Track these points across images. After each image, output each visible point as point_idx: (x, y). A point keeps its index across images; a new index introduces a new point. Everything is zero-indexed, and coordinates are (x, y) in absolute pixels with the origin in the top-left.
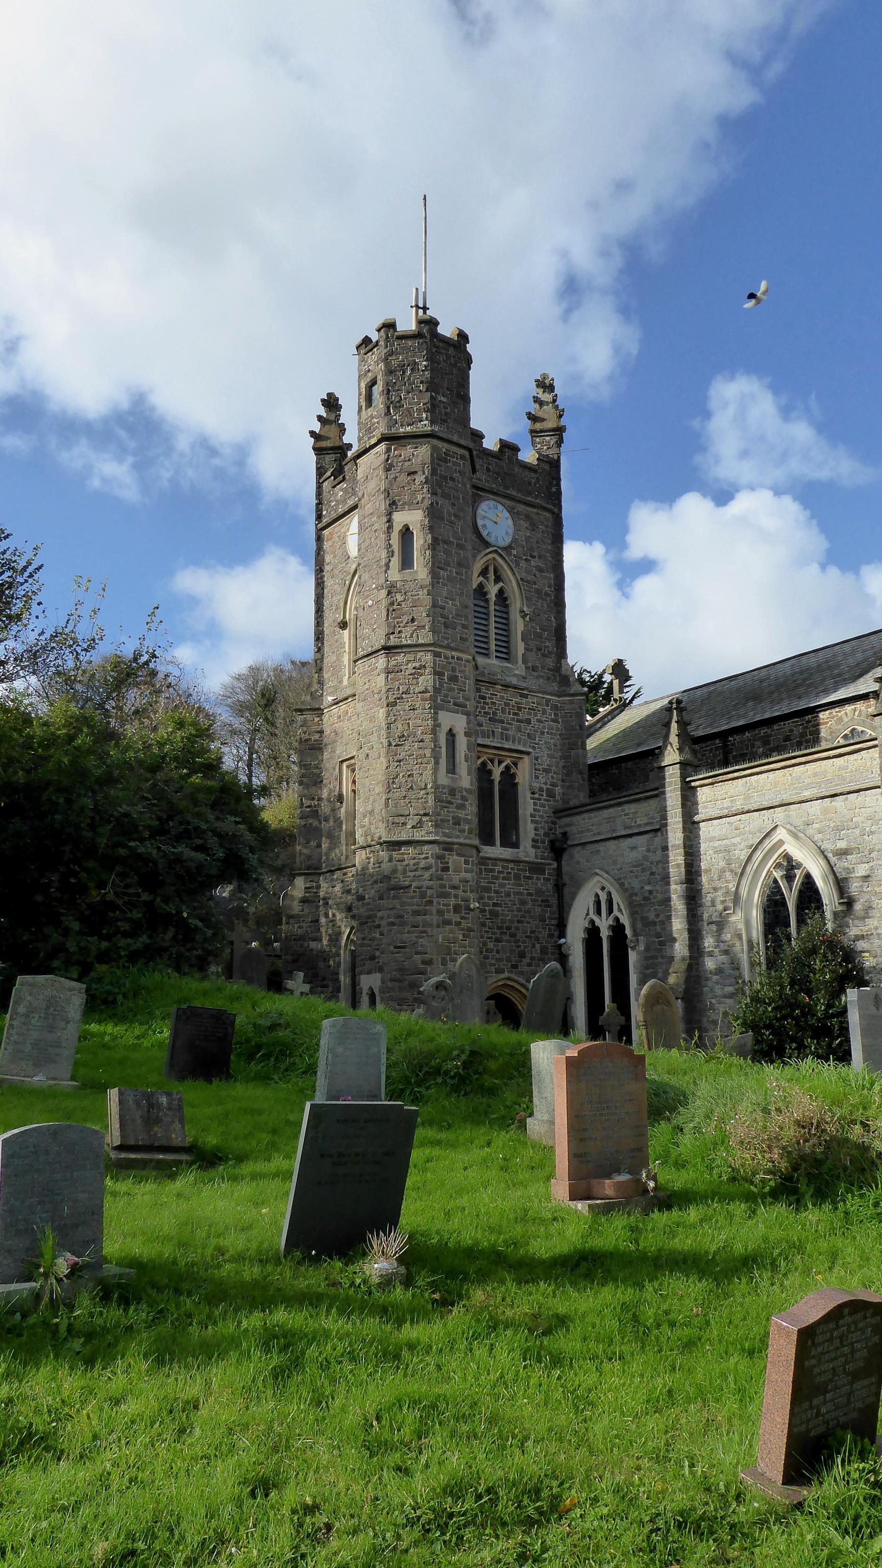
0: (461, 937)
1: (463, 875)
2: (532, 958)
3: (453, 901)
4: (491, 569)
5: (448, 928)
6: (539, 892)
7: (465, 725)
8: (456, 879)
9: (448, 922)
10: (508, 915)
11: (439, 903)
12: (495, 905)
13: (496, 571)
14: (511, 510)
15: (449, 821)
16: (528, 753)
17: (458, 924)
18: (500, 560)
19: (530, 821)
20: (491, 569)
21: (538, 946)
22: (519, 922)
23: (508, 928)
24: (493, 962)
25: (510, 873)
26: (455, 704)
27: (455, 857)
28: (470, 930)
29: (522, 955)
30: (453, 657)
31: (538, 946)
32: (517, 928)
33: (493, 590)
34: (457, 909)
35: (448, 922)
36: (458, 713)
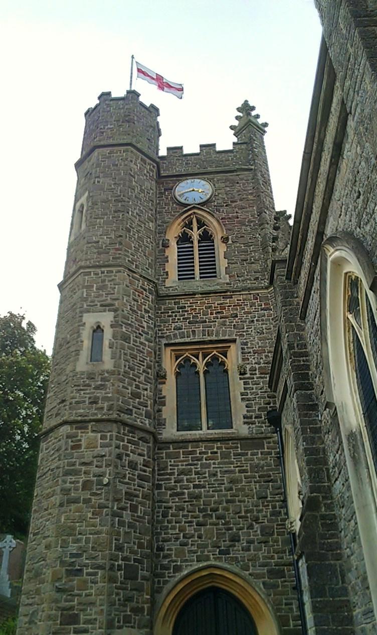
0: (90, 515)
1: (99, 450)
2: (250, 542)
3: (83, 478)
4: (194, 220)
5: (73, 507)
6: (256, 468)
7: (112, 319)
8: (88, 456)
9: (76, 501)
10: (213, 496)
11: (65, 482)
12: (195, 487)
13: (199, 221)
14: (209, 180)
15: (84, 402)
16: (234, 341)
17: (87, 501)
18: (200, 212)
19: (240, 400)
20: (194, 220)
21: (256, 526)
22: (228, 502)
23: (215, 510)
24: (194, 548)
25: (216, 453)
26: (101, 306)
27: (90, 434)
28: (101, 507)
29: (235, 539)
30: (103, 272)
31: (256, 526)
32: (227, 509)
33: (195, 234)
34: (86, 485)
35: (76, 501)
36: (105, 311)
